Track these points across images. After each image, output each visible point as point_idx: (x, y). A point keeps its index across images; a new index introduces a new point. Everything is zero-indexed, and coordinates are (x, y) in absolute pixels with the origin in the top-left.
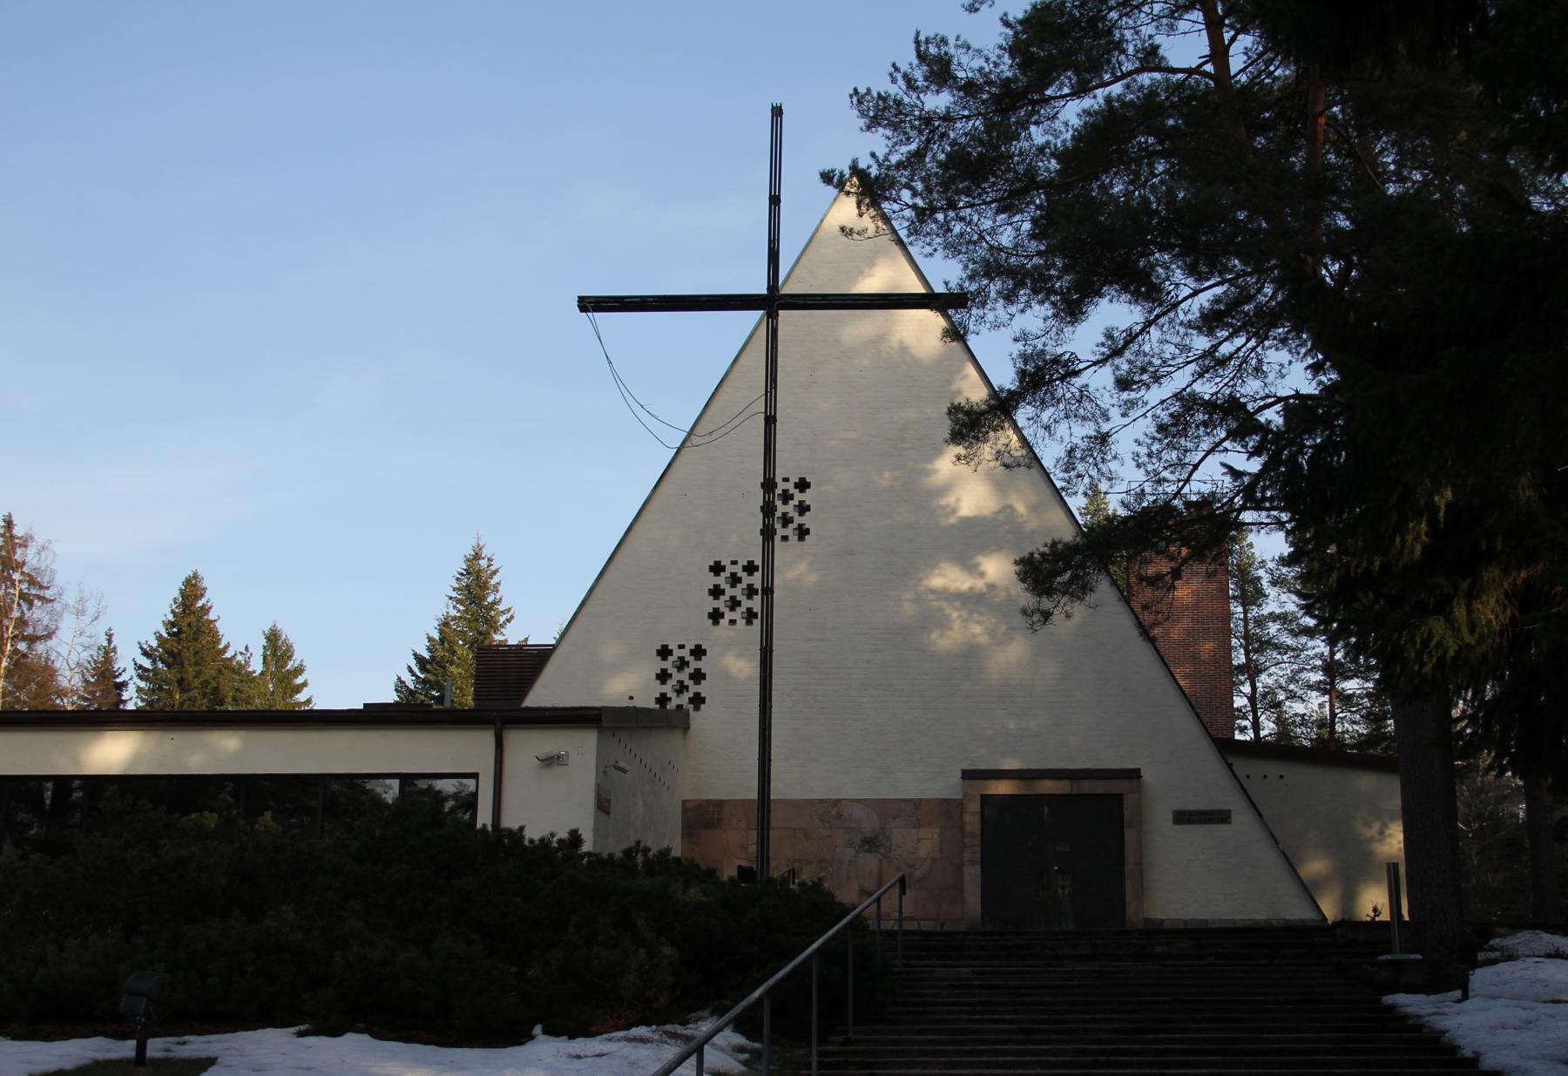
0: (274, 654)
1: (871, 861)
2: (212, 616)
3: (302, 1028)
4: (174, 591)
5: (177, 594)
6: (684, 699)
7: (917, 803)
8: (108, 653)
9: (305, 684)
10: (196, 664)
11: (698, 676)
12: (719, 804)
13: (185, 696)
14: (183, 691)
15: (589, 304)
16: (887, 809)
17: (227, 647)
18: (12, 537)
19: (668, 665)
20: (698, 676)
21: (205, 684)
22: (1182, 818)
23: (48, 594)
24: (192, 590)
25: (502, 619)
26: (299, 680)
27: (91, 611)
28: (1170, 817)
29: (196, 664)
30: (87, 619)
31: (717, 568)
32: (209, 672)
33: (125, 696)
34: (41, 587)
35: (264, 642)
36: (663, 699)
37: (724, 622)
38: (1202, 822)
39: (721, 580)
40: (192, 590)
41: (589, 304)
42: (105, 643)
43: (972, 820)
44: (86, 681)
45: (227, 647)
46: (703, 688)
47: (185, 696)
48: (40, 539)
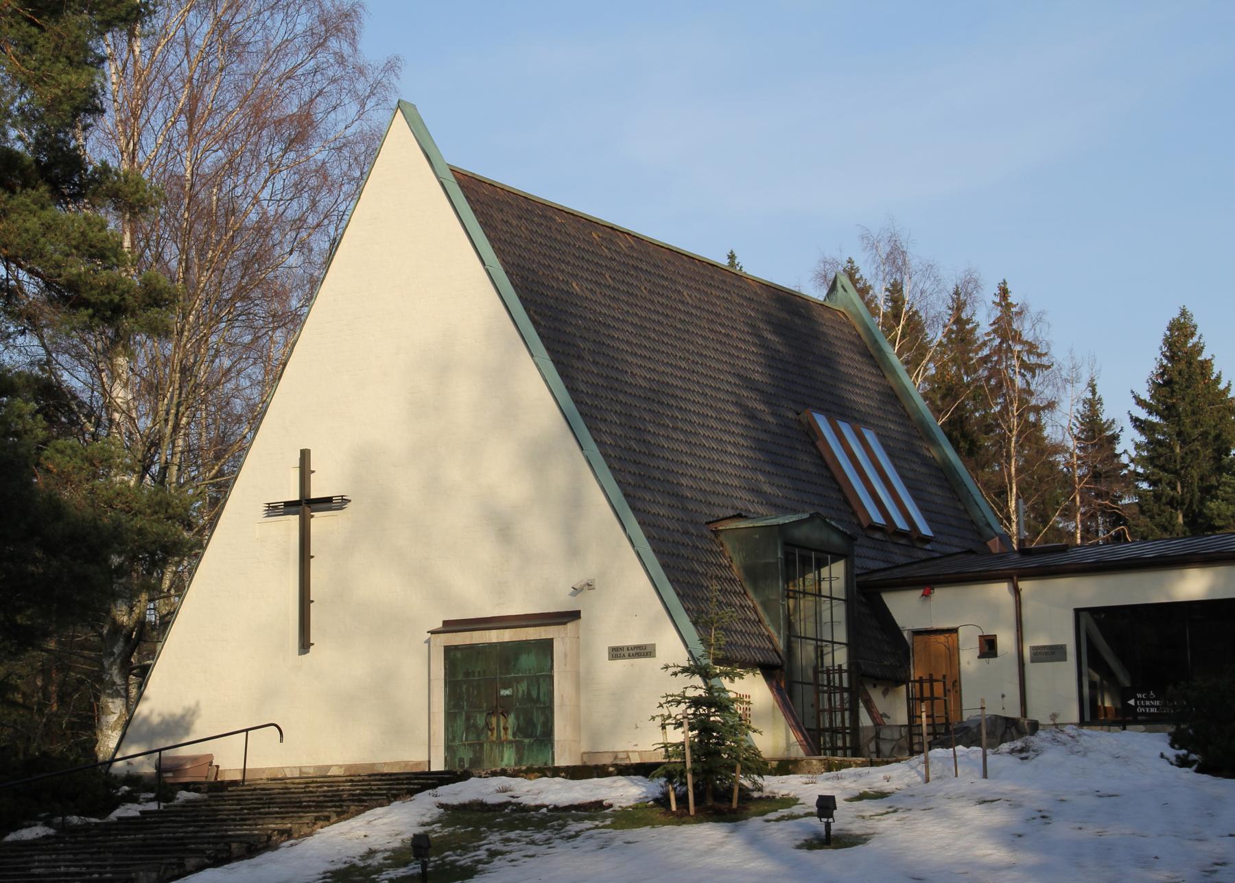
2: (1205, 356)
8: (1093, 404)
10: (1193, 413)
13: (1186, 449)
14: (1184, 443)
18: (1009, 306)
21: (1205, 435)
22: (616, 653)
23: (1045, 361)
28: (828, 793)
29: (1193, 413)
32: (1209, 420)
33: (1119, 449)
34: (1039, 355)
42: (1090, 396)
47: (1186, 449)
48: (1033, 309)
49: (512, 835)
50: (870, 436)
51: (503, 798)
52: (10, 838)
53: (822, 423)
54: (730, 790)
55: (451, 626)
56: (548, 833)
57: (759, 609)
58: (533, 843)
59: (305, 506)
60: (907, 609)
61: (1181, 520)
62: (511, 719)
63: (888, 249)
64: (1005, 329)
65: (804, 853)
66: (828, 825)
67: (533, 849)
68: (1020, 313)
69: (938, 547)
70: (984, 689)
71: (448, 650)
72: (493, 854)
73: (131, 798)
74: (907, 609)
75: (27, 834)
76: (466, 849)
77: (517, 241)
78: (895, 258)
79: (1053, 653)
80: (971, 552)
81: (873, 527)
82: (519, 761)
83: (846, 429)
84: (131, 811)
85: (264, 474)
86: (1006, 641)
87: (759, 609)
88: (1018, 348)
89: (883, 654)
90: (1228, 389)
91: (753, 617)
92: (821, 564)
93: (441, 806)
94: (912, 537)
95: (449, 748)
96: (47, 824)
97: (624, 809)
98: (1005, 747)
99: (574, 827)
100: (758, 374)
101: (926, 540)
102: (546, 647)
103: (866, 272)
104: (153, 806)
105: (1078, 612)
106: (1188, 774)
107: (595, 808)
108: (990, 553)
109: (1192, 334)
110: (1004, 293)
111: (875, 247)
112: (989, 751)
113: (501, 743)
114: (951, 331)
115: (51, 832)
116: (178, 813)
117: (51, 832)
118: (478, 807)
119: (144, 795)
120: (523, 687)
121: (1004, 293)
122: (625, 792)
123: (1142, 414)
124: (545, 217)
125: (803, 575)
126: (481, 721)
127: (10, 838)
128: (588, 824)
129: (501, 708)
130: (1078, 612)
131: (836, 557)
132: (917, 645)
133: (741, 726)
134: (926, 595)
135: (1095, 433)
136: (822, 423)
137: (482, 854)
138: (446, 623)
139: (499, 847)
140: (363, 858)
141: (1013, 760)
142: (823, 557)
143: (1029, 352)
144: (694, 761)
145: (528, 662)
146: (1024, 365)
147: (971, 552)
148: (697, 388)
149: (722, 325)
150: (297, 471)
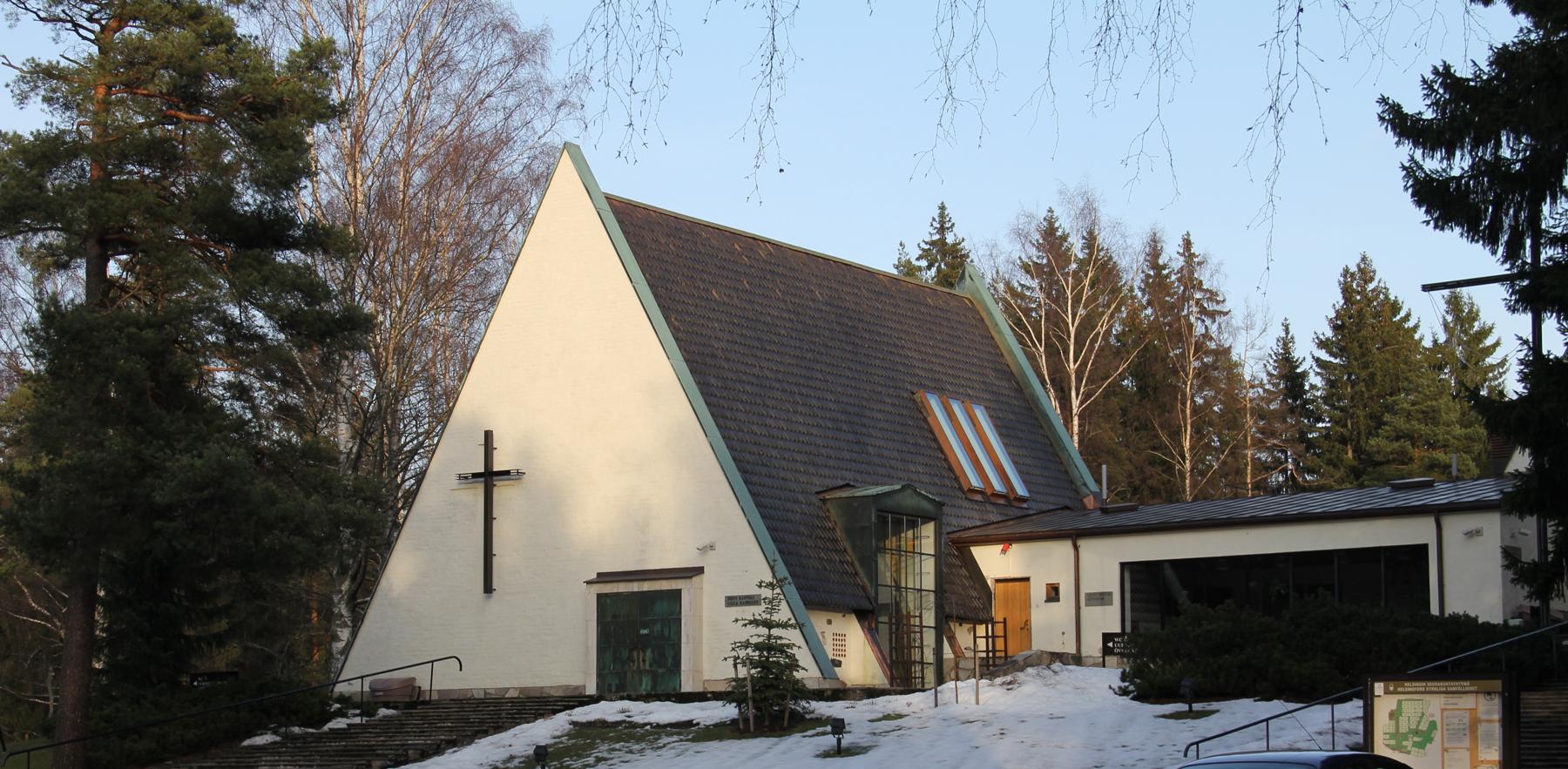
0: (1458, 318)
8: (1286, 342)
9: (1497, 344)
17: (1408, 316)
18: (1192, 255)
27: (1259, 325)
29: (1363, 355)
30: (1255, 333)
38: (742, 604)
44: (1269, 374)
45: (1408, 316)
48: (1213, 262)
49: (617, 746)
50: (980, 414)
51: (620, 717)
53: (934, 403)
54: (782, 712)
55: (604, 578)
56: (643, 745)
57: (857, 564)
58: (631, 752)
59: (489, 477)
60: (993, 562)
61: (1350, 454)
62: (649, 653)
63: (1081, 204)
64: (1189, 280)
65: (818, 760)
66: (839, 740)
67: (629, 756)
68: (1200, 264)
69: (1034, 505)
70: (1049, 625)
71: (599, 596)
72: (599, 760)
73: (341, 714)
74: (993, 562)
75: (259, 740)
76: (580, 756)
77: (665, 257)
78: (1088, 211)
79: (1102, 599)
80: (1067, 508)
81: (973, 491)
82: (654, 687)
83: (957, 408)
84: (339, 723)
85: (453, 455)
86: (1066, 591)
87: (857, 564)
88: (1198, 296)
89: (964, 597)
90: (1416, 327)
91: (849, 569)
92: (913, 525)
93: (574, 723)
94: (1010, 499)
95: (600, 675)
96: (275, 733)
97: (707, 727)
98: (999, 680)
99: (665, 740)
102: (676, 595)
103: (1065, 223)
104: (357, 720)
105: (1123, 565)
108: (1085, 508)
109: (1372, 279)
110: (1187, 244)
112: (984, 682)
113: (640, 672)
114: (1148, 276)
115: (278, 739)
116: (375, 726)
117: (278, 739)
118: (603, 724)
119: (351, 712)
120: (658, 627)
121: (1187, 244)
123: (1324, 355)
124: (692, 233)
125: (897, 533)
126: (625, 654)
127: (246, 743)
128: (675, 738)
129: (641, 644)
130: (1123, 565)
131: (927, 518)
133: (794, 665)
134: (1004, 551)
135: (1289, 373)
137: (591, 760)
138: (599, 574)
139: (605, 755)
140: (505, 762)
141: (1002, 690)
142: (916, 519)
143: (1210, 299)
145: (661, 607)
146: (1203, 311)
147: (1067, 508)
148: (819, 376)
149: (850, 318)
150: (482, 449)
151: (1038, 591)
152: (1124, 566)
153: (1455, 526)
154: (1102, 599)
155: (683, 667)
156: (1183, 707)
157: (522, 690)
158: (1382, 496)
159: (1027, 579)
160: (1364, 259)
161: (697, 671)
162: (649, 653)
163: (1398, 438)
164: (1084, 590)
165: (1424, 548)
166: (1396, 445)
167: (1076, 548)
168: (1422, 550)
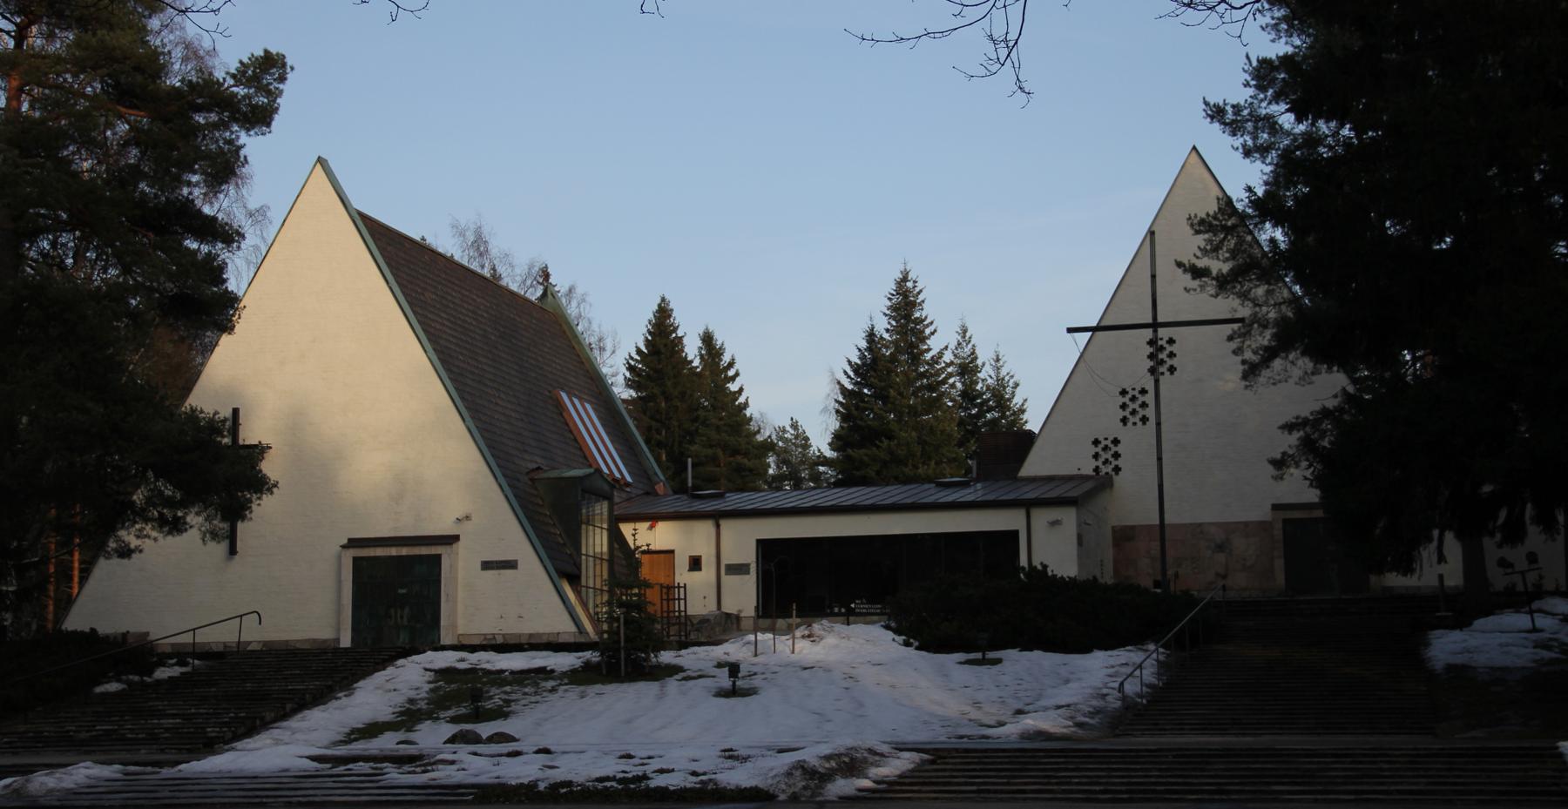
1: (1221, 557)
3: (972, 656)
4: (648, 312)
5: (651, 316)
6: (1109, 469)
7: (1246, 524)
11: (1116, 456)
12: (1133, 527)
15: (1070, 330)
16: (1229, 528)
19: (1099, 449)
20: (1116, 456)
24: (663, 313)
25: (928, 331)
26: (731, 373)
27: (609, 347)
31: (1124, 393)
35: (700, 344)
36: (1097, 469)
37: (1130, 424)
39: (1126, 399)
40: (663, 313)
41: (1070, 330)
43: (1278, 532)
46: (1120, 462)
52: (99, 690)
53: (564, 396)
55: (353, 543)
71: (355, 560)
79: (738, 569)
84: (162, 673)
96: (119, 681)
100: (856, 360)
101: (628, 484)
106: (911, 651)
107: (543, 672)
111: (462, 234)
122: (563, 662)
127: (99, 690)
132: (645, 559)
134: (651, 527)
136: (564, 396)
144: (46, 606)
151: (682, 562)
152: (759, 541)
153: (1041, 517)
154: (738, 569)
155: (443, 623)
156: (979, 655)
157: (265, 643)
158: (932, 494)
159: (672, 552)
160: (663, 299)
161: (454, 626)
162: (407, 610)
163: (711, 446)
164: (724, 562)
165: (1015, 534)
166: (710, 452)
167: (718, 526)
168: (1014, 535)
